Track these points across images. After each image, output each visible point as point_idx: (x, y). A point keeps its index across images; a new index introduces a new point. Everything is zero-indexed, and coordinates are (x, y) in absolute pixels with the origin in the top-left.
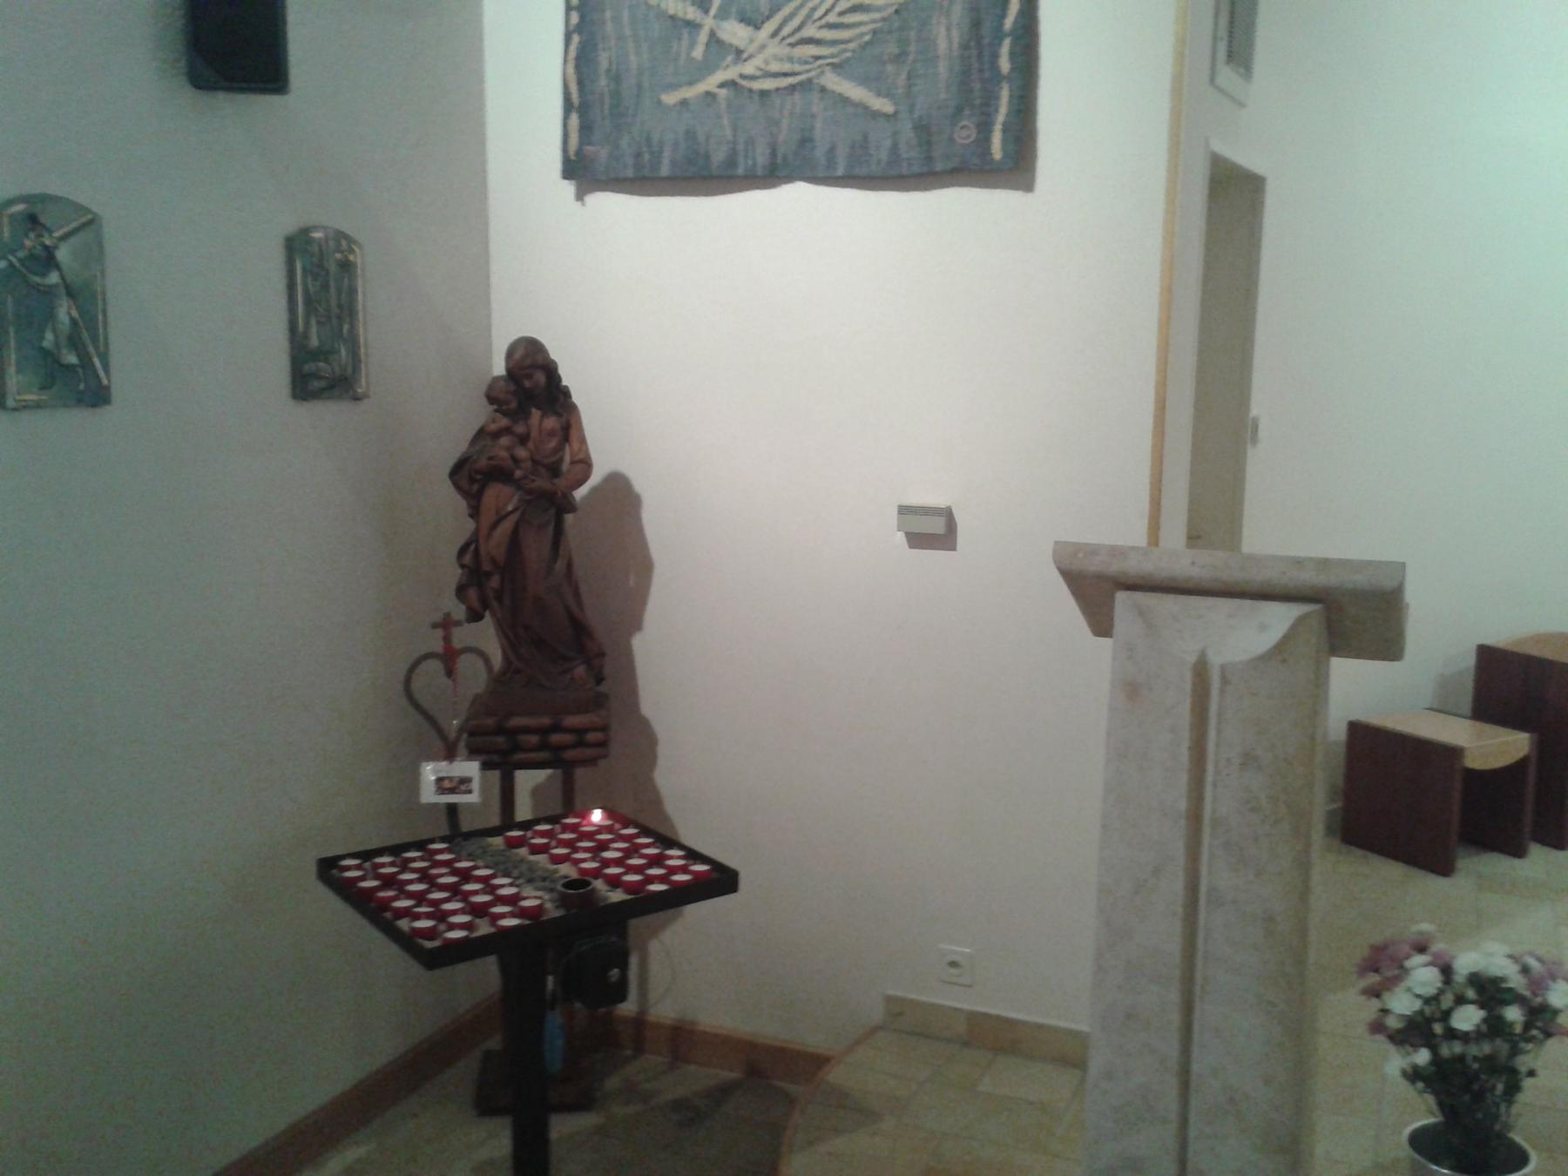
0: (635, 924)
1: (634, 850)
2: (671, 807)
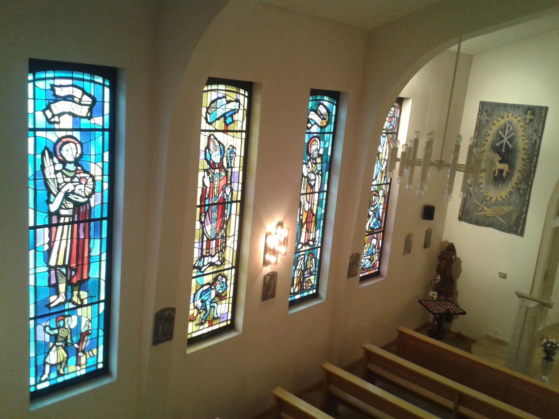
0: (454, 316)
1: (454, 307)
2: (459, 301)
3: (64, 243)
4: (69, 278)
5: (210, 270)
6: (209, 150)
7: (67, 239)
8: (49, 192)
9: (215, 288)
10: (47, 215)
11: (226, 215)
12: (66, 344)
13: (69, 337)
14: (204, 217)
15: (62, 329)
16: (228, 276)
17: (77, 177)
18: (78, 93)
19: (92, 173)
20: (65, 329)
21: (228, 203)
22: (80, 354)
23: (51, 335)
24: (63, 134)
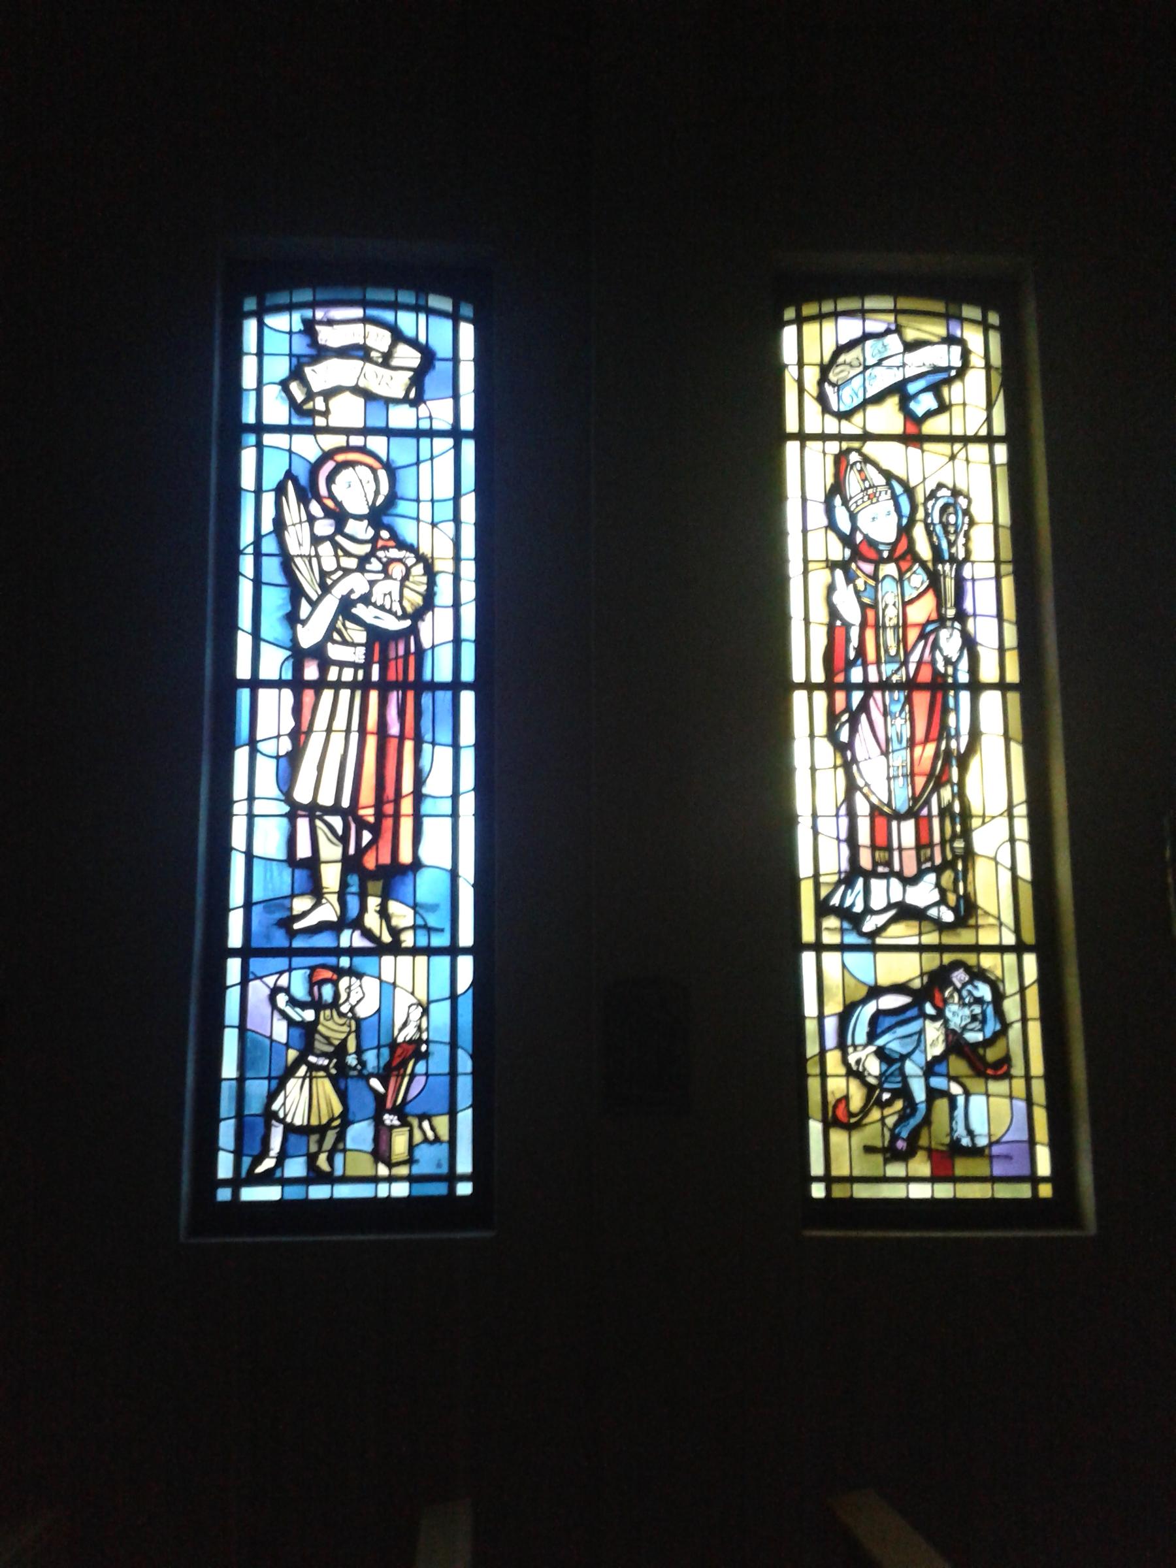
3: (337, 739)
4: (352, 851)
5: (903, 933)
6: (845, 503)
7: (348, 731)
8: (296, 592)
9: (940, 1015)
10: (288, 653)
11: (953, 732)
12: (342, 1067)
13: (352, 1046)
14: (847, 726)
15: (328, 1012)
16: (1003, 981)
17: (379, 559)
18: (379, 339)
19: (425, 549)
20: (341, 1015)
21: (957, 687)
22: (389, 1119)
23: (291, 1023)
24: (340, 441)
